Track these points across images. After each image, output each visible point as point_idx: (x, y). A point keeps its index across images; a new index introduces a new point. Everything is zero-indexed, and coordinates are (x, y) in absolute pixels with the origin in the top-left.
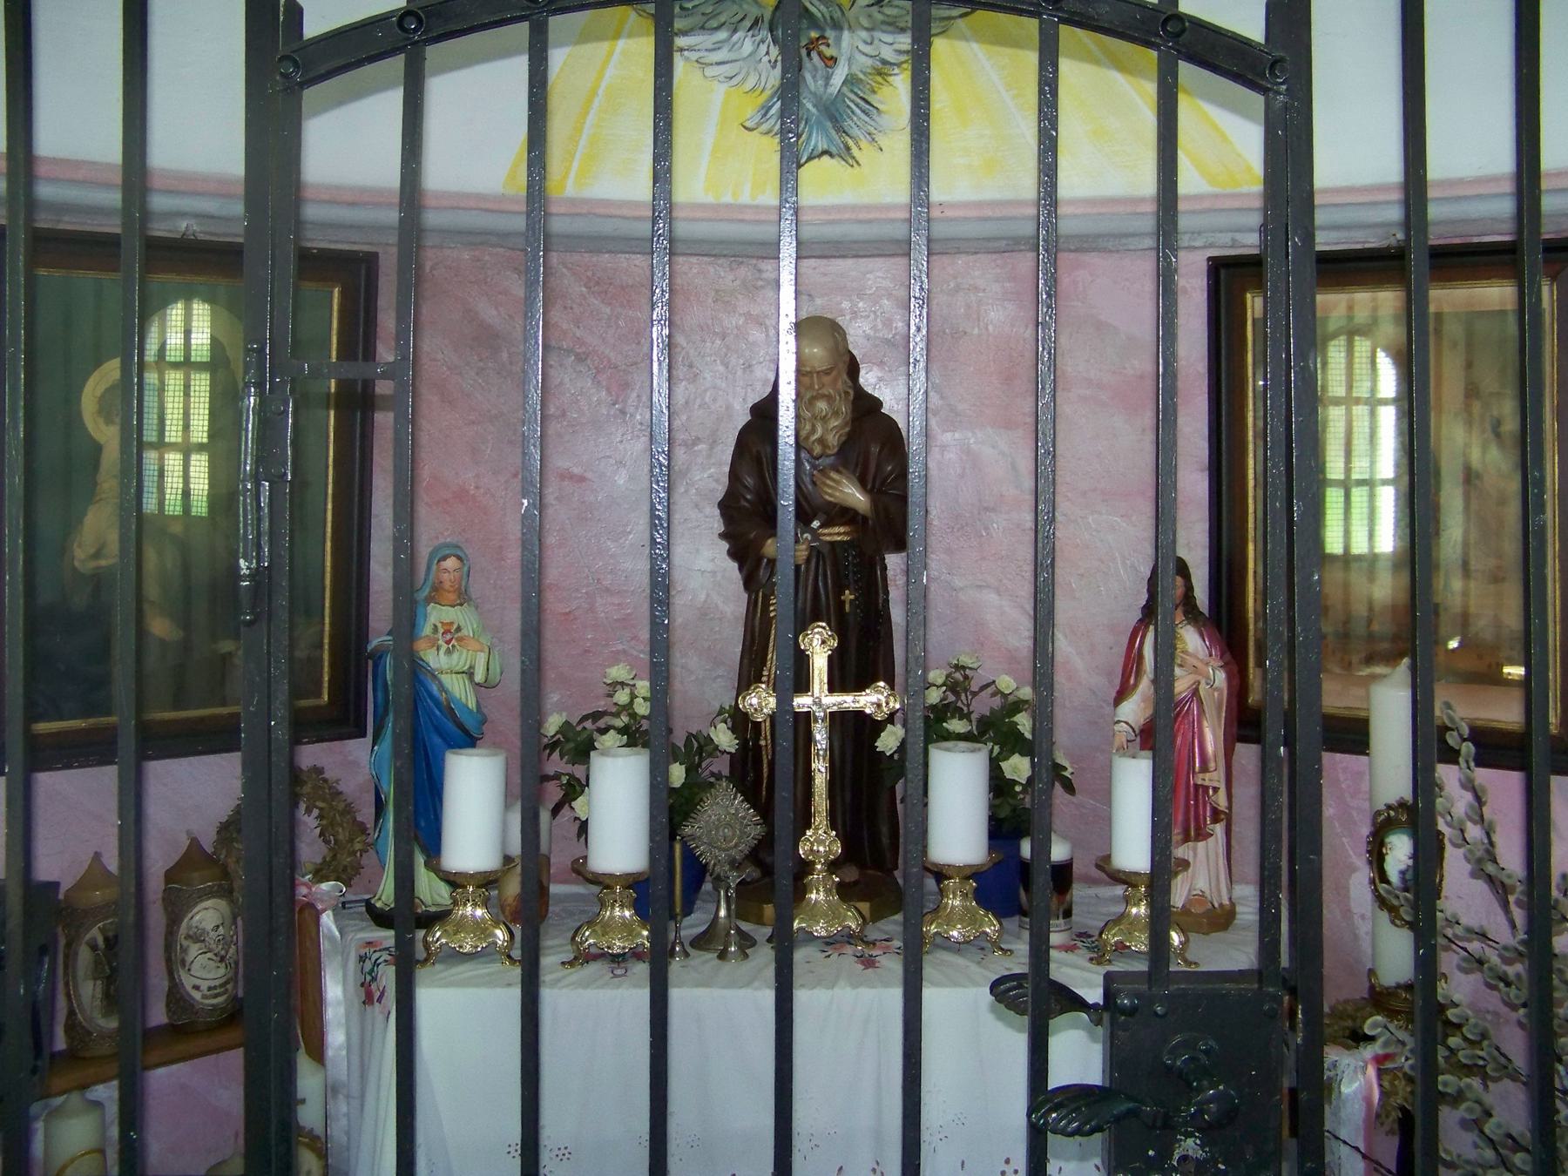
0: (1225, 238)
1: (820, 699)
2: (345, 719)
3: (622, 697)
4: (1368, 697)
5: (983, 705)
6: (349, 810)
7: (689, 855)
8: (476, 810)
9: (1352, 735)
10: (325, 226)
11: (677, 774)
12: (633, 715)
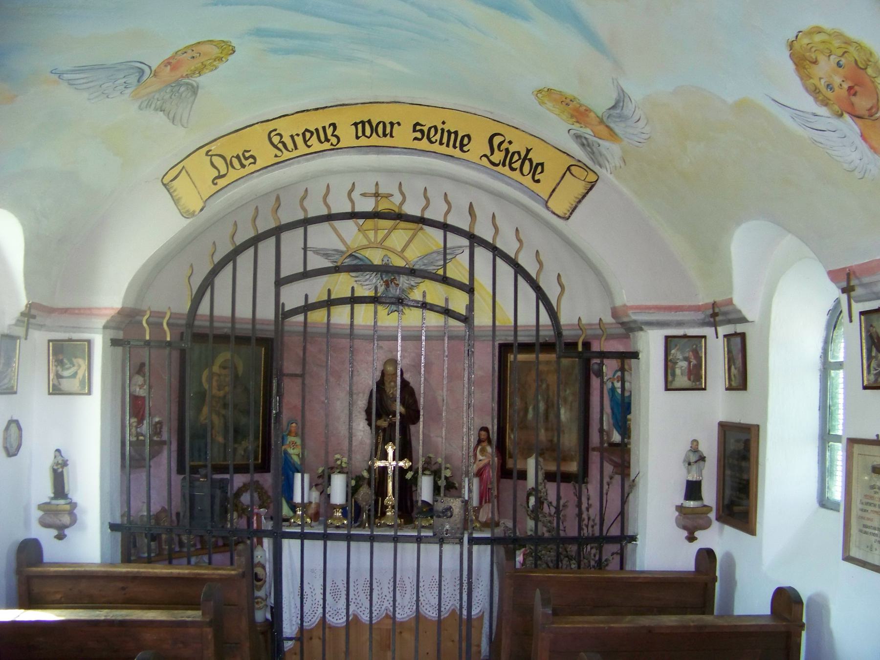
0: (503, 338)
1: (391, 463)
2: (264, 467)
3: (339, 462)
4: (526, 463)
5: (434, 468)
6: (266, 492)
7: (355, 502)
8: (301, 489)
9: (523, 475)
10: (262, 330)
11: (353, 483)
12: (342, 468)
